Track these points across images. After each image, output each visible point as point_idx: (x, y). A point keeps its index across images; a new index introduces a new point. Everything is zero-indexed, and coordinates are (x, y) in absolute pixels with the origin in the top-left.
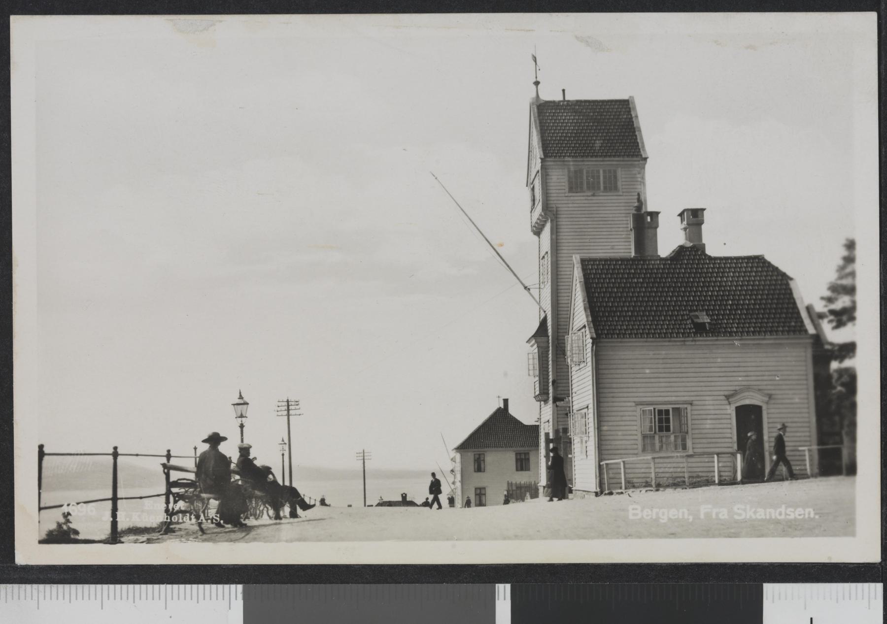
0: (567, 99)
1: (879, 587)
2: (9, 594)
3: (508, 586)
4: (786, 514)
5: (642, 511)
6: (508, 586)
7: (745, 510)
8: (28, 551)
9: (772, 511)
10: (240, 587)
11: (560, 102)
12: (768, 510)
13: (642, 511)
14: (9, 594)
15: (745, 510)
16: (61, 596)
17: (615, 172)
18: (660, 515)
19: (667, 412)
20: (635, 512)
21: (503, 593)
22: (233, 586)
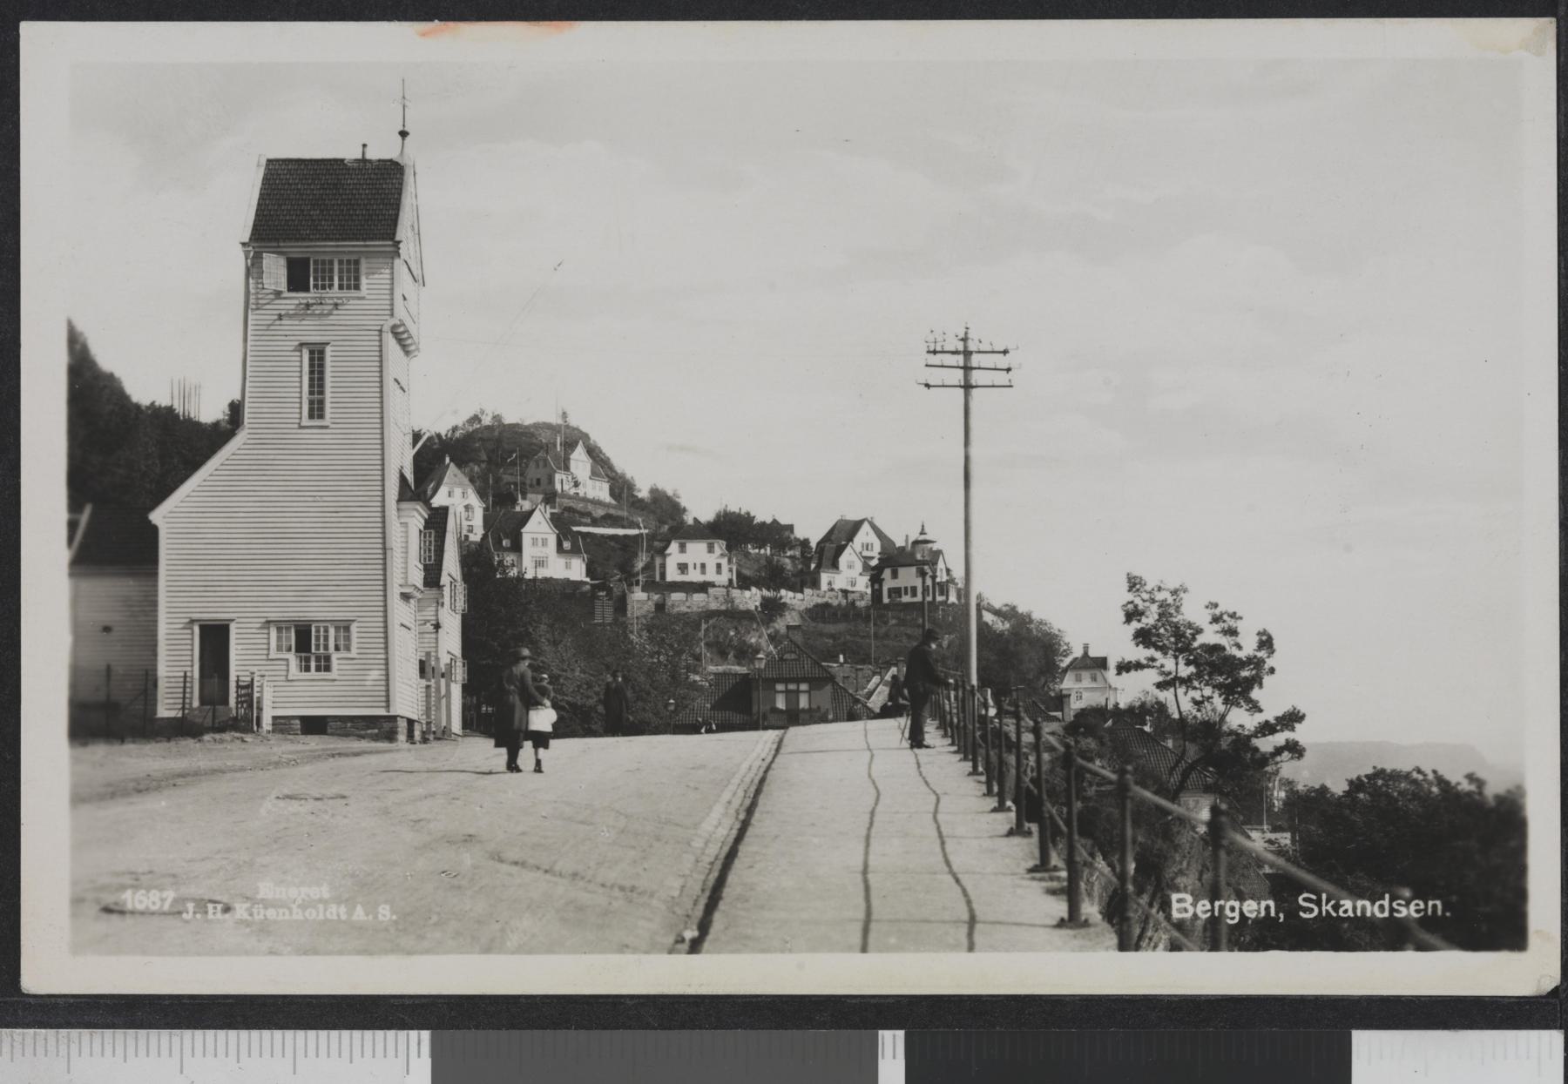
0: (368, 157)
1: (1557, 1037)
2: (18, 1046)
3: (901, 1034)
4: (1392, 910)
5: (1194, 905)
6: (901, 1034)
7: (1318, 903)
8: (46, 967)
9: (1367, 903)
10: (426, 1035)
11: (357, 161)
12: (1360, 903)
13: (1194, 905)
14: (18, 1046)
15: (1318, 903)
16: (165, 1052)
17: (357, 262)
18: (1228, 912)
19: (318, 669)
20: (1182, 905)
21: (892, 1046)
22: (413, 1034)
